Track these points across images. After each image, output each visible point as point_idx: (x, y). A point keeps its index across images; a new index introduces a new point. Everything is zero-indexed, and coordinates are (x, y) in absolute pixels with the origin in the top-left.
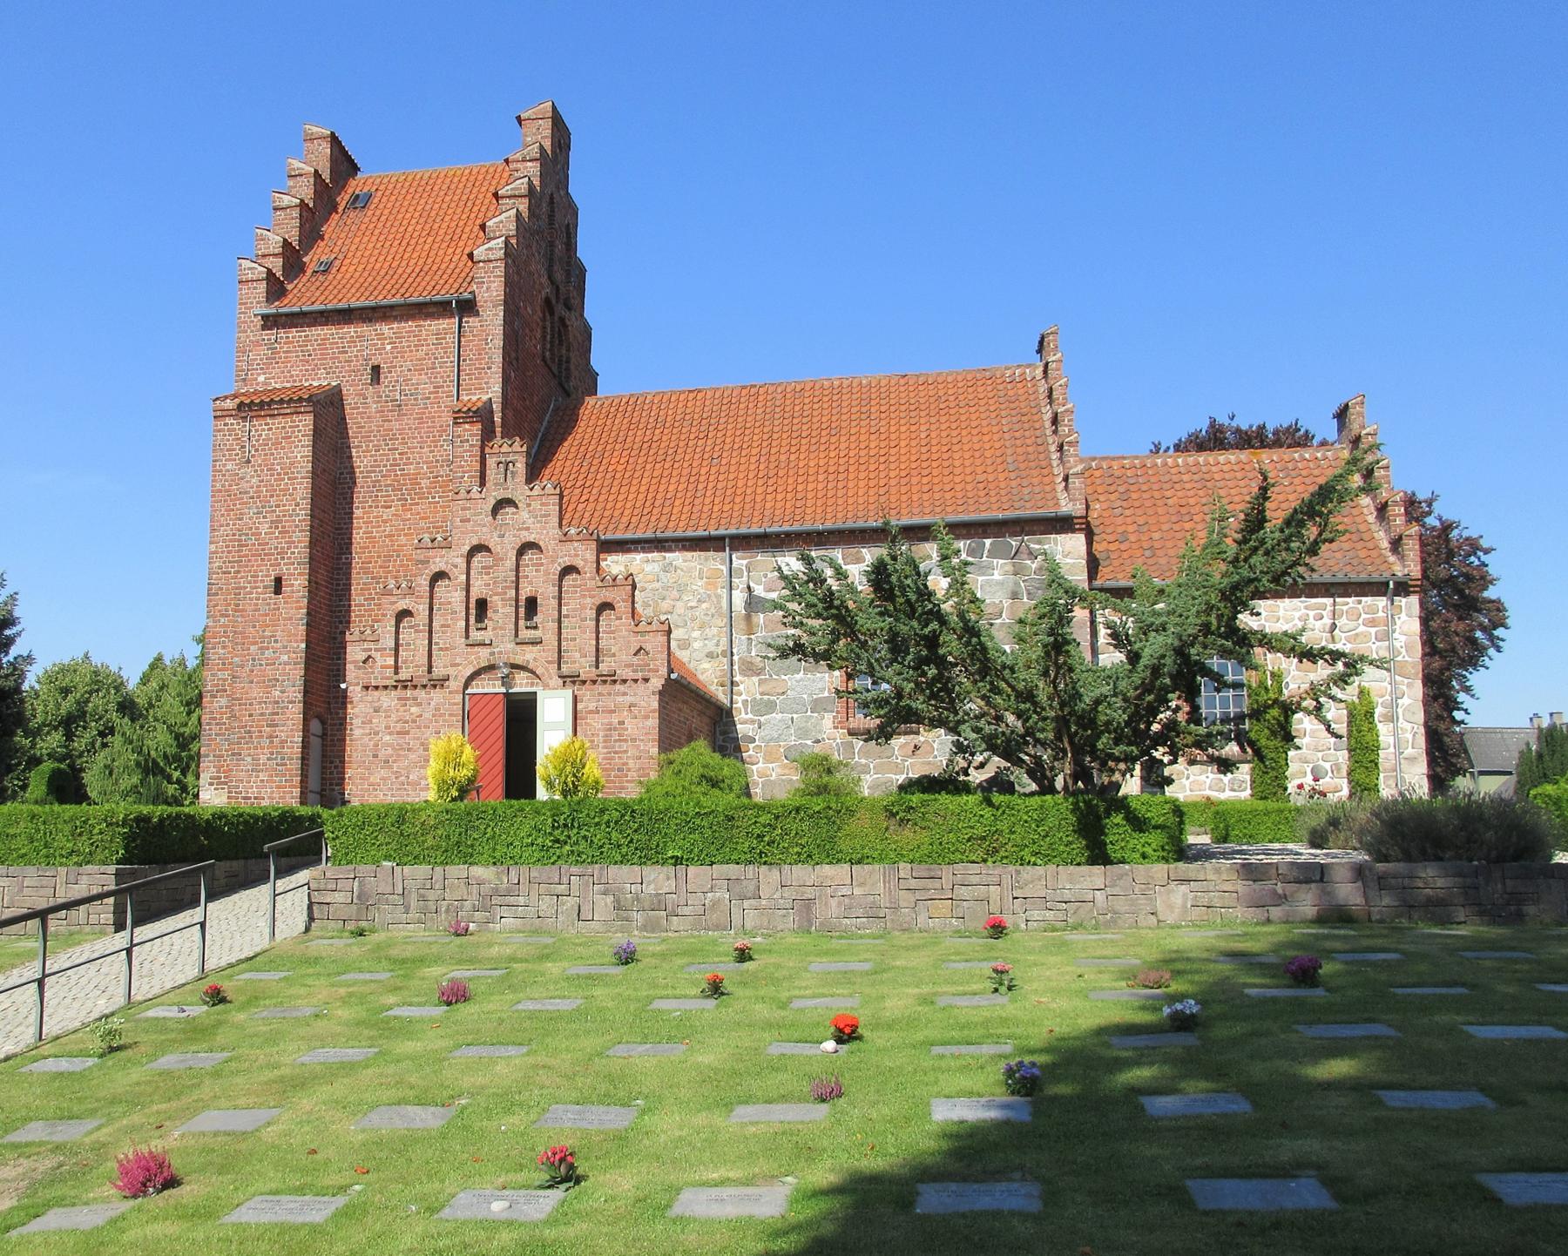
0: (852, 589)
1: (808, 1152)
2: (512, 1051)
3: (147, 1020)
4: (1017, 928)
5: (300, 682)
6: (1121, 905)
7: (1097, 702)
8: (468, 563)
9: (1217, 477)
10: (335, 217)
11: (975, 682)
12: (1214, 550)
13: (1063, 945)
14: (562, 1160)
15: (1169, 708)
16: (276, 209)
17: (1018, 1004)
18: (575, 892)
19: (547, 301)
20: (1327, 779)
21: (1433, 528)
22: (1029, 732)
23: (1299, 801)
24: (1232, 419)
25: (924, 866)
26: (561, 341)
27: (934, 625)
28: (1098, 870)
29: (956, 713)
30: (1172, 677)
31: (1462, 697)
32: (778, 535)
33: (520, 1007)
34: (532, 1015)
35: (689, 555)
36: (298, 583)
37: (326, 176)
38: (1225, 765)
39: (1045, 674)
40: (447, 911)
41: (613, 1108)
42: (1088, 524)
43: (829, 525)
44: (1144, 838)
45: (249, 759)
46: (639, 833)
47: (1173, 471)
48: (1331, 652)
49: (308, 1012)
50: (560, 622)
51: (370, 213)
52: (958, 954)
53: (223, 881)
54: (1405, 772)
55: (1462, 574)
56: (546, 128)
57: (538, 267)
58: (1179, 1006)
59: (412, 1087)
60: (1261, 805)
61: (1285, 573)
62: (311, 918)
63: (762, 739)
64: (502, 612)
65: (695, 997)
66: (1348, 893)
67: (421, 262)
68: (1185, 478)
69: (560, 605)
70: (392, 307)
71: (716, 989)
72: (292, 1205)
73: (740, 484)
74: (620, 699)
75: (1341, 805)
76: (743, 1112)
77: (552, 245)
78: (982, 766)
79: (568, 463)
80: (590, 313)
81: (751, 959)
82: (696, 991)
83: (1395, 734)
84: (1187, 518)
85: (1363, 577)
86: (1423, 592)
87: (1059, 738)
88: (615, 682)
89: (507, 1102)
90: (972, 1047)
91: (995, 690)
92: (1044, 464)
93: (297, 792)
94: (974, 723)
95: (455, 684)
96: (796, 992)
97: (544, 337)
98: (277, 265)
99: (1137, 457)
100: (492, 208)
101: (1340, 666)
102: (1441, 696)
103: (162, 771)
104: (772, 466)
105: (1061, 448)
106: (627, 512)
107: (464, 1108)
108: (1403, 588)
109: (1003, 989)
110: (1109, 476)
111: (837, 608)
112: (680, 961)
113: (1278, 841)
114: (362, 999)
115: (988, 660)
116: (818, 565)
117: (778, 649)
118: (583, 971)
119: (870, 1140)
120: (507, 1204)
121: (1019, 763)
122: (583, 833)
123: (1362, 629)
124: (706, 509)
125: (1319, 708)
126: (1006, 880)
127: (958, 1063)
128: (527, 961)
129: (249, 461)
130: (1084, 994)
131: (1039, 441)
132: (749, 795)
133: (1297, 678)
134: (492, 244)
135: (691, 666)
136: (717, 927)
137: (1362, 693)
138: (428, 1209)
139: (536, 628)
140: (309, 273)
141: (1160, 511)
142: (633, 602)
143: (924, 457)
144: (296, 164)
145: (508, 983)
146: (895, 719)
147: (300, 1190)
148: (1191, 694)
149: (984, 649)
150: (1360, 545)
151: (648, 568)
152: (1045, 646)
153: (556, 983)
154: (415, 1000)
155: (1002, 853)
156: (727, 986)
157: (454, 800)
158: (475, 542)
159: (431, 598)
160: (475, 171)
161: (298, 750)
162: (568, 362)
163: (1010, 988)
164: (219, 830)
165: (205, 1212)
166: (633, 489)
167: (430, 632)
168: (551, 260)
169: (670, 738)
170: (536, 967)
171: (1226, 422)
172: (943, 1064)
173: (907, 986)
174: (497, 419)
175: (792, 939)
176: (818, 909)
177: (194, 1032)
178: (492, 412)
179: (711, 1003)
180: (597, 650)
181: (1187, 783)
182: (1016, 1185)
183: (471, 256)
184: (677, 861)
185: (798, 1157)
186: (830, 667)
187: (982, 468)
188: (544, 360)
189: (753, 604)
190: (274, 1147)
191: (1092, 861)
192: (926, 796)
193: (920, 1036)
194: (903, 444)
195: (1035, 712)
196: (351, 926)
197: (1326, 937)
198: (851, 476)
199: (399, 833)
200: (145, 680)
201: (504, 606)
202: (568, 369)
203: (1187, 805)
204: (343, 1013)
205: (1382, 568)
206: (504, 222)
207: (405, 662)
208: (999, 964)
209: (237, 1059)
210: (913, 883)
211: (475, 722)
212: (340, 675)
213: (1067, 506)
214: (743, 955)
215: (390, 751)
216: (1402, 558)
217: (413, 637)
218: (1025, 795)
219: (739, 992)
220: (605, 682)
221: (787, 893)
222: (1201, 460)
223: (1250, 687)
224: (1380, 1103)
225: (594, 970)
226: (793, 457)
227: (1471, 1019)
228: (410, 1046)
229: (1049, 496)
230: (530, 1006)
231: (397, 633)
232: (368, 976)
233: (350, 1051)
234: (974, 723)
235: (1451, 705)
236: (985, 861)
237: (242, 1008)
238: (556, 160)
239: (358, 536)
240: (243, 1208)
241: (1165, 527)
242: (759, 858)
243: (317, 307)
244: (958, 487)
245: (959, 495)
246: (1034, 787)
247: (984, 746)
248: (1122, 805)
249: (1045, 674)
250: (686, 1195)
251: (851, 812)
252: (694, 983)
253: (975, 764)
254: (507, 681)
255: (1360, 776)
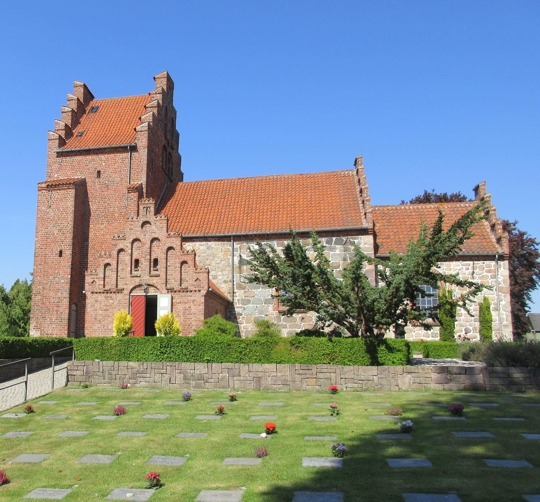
0: (278, 257)
1: (251, 477)
2: (140, 434)
3: (3, 418)
4: (342, 390)
5: (68, 290)
6: (384, 382)
7: (374, 301)
8: (132, 245)
9: (426, 213)
10: (85, 115)
11: (325, 293)
12: (421, 241)
13: (360, 398)
14: (154, 478)
15: (404, 304)
16: (63, 112)
17: (341, 420)
18: (168, 372)
19: (164, 146)
20: (471, 333)
21: (516, 235)
22: (347, 313)
23: (459, 341)
24: (433, 191)
25: (305, 365)
26: (169, 162)
27: (309, 270)
28: (375, 368)
29: (318, 305)
30: (404, 291)
31: (528, 302)
32: (251, 235)
33: (145, 417)
34: (149, 420)
35: (217, 243)
36: (68, 253)
37: (82, 100)
38: (427, 327)
39: (353, 289)
40: (120, 379)
41: (177, 457)
42: (374, 232)
43: (271, 232)
44: (393, 355)
45: (49, 319)
46: (193, 350)
47: (408, 211)
48: (469, 283)
49: (64, 416)
50: (167, 268)
51: (98, 114)
52: (318, 400)
53: (36, 366)
54: (503, 331)
55: (527, 253)
56: (165, 81)
57: (161, 133)
58: (404, 423)
59: (100, 447)
60: (443, 343)
61: (450, 251)
62: (68, 381)
63: (245, 314)
64: (144, 264)
65: (213, 415)
66: (480, 378)
67: (117, 132)
68: (413, 214)
69: (167, 262)
70: (105, 149)
71: (221, 411)
72: (50, 492)
73: (237, 216)
74: (189, 298)
75: (476, 343)
76: (228, 461)
77: (166, 125)
78: (329, 326)
79: (171, 208)
80: (180, 151)
81: (236, 400)
82: (213, 412)
83: (499, 315)
84: (414, 230)
85: (485, 253)
86: (510, 258)
87: (359, 315)
88: (187, 291)
89: (136, 454)
90: (321, 437)
91: (334, 296)
92: (357, 208)
93: (66, 332)
94: (325, 309)
95: (126, 292)
96: (253, 414)
97: (163, 160)
98: (63, 133)
99: (394, 206)
100: (144, 111)
101: (473, 288)
102: (518, 298)
103: (17, 323)
104: (250, 209)
105: (363, 202)
106: (193, 227)
107: (120, 456)
108: (501, 258)
109: (335, 414)
110: (382, 213)
111: (271, 263)
112: (208, 400)
113: (450, 357)
114: (85, 412)
115: (330, 284)
116: (264, 247)
117: (248, 279)
118: (170, 403)
119: (277, 473)
120: (132, 494)
121: (344, 325)
122: (172, 349)
123: (485, 274)
124: (224, 225)
125: (465, 304)
126: (338, 371)
127: (314, 443)
128: (149, 399)
129: (50, 207)
130: (367, 417)
131: (355, 199)
132: (240, 336)
133: (457, 292)
134: (144, 124)
135: (218, 286)
136: (223, 387)
137: (485, 299)
138: (102, 495)
139: (157, 270)
140: (75, 136)
141: (403, 227)
142: (195, 261)
143: (309, 206)
144: (71, 96)
145: (141, 407)
146: (293, 307)
147: (54, 486)
148: (413, 298)
149: (329, 280)
150: (484, 241)
151: (201, 248)
152: (352, 279)
153: (159, 408)
154: (105, 413)
155: (336, 360)
156: (225, 410)
157: (123, 336)
158: (135, 238)
159: (118, 259)
160: (138, 98)
161: (67, 316)
162: (172, 169)
163: (337, 414)
164: (35, 346)
165: (18, 494)
166: (196, 218)
167: (117, 272)
168: (166, 131)
169: (208, 314)
170: (152, 401)
171: (431, 192)
172: (309, 444)
173: (297, 412)
174: (144, 191)
175: (253, 393)
176: (263, 382)
177: (20, 423)
178: (142, 188)
179: (219, 417)
180: (181, 279)
181: (414, 334)
182: (333, 493)
183: (135, 129)
184: (208, 361)
185: (248, 479)
186: (269, 286)
187: (332, 210)
188: (163, 168)
189: (242, 262)
190: (47, 469)
191: (372, 364)
192: (306, 338)
193: (300, 432)
194: (301, 200)
195: (350, 305)
196: (82, 384)
197: (472, 396)
198: (280, 213)
199: (102, 348)
200: (12, 289)
201: (145, 262)
202: (172, 172)
203: (413, 343)
204: (77, 418)
205: (493, 250)
206: (148, 117)
207: (108, 283)
208: (333, 404)
209: (35, 434)
210: (301, 372)
211: (134, 306)
212: (83, 288)
213: (366, 224)
214: (233, 399)
215: (101, 317)
216: (501, 246)
217: (111, 274)
218: (346, 337)
219: (230, 413)
220: (184, 291)
221: (251, 374)
222: (420, 207)
223: (439, 296)
224: (485, 464)
225: (174, 403)
226: (258, 206)
227: (524, 431)
228: (101, 431)
229: (358, 221)
230: (149, 417)
231: (105, 272)
232: (88, 404)
233: (78, 432)
234: (325, 309)
235: (524, 305)
236: (329, 363)
237: (39, 415)
238: (168, 93)
239: (91, 235)
240: (32, 493)
241: (405, 233)
242: (240, 360)
243: (77, 149)
244: (322, 217)
245: (323, 220)
246: (349, 334)
247: (329, 318)
248: (384, 342)
249: (353, 289)
250: (203, 493)
251: (276, 343)
252: (213, 409)
253: (327, 325)
254: (146, 291)
255: (484, 332)
